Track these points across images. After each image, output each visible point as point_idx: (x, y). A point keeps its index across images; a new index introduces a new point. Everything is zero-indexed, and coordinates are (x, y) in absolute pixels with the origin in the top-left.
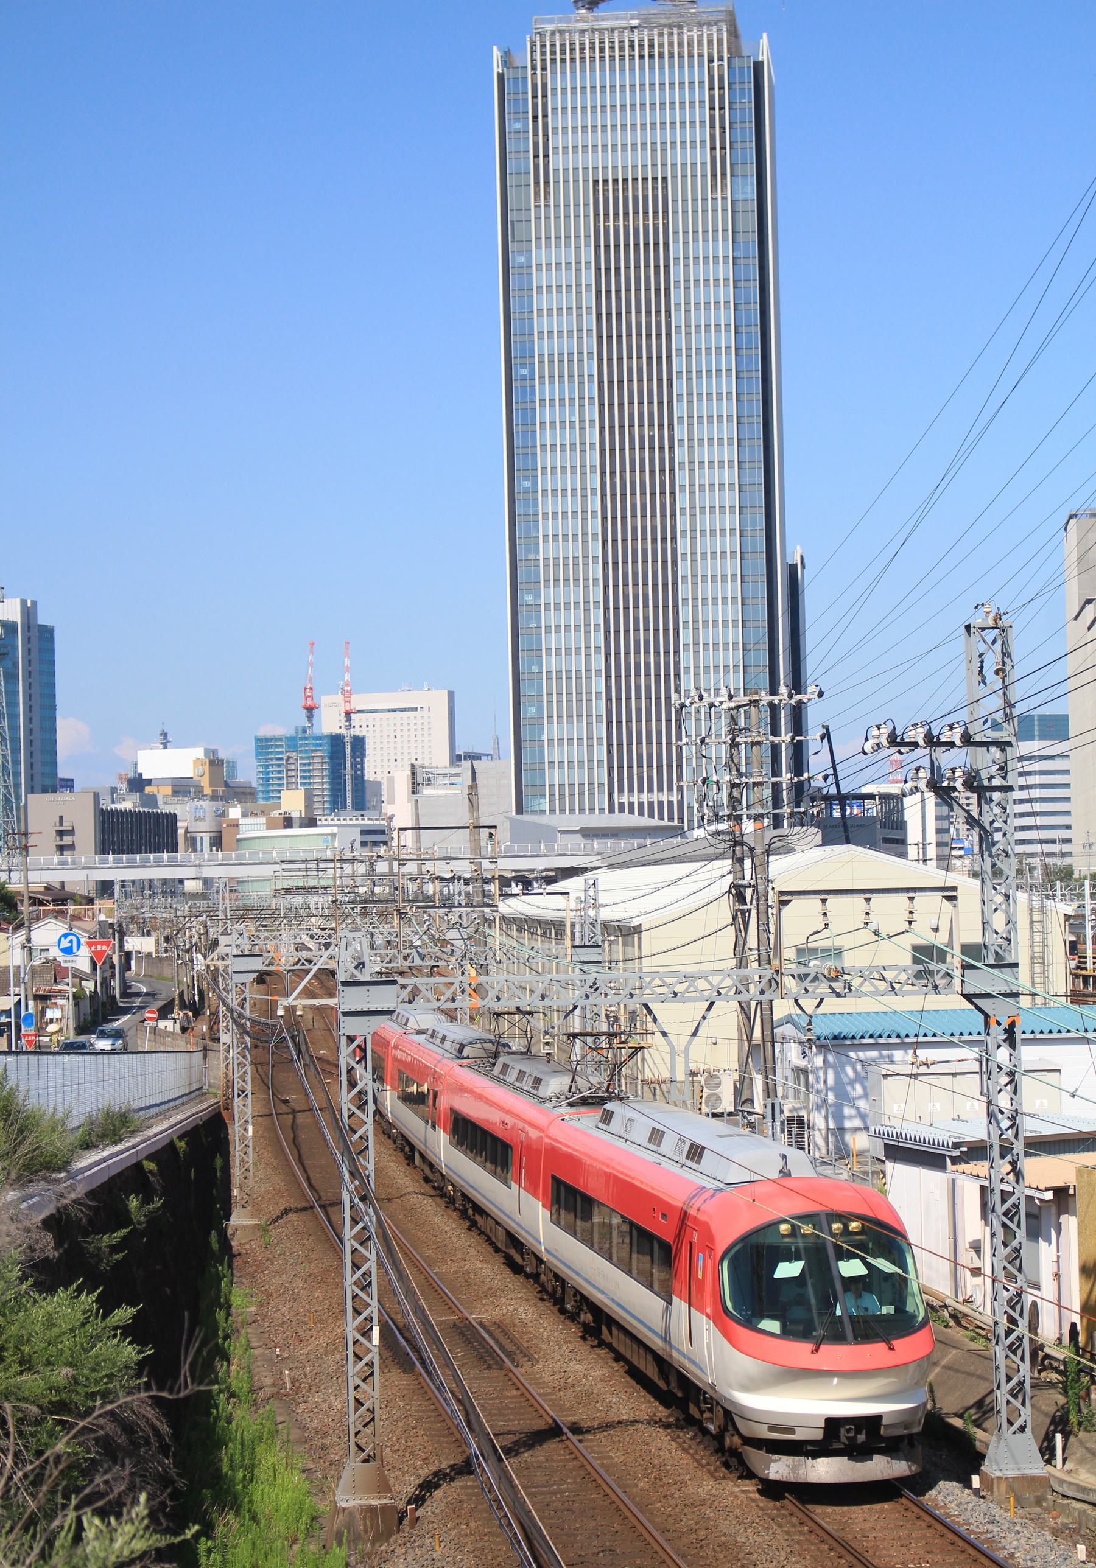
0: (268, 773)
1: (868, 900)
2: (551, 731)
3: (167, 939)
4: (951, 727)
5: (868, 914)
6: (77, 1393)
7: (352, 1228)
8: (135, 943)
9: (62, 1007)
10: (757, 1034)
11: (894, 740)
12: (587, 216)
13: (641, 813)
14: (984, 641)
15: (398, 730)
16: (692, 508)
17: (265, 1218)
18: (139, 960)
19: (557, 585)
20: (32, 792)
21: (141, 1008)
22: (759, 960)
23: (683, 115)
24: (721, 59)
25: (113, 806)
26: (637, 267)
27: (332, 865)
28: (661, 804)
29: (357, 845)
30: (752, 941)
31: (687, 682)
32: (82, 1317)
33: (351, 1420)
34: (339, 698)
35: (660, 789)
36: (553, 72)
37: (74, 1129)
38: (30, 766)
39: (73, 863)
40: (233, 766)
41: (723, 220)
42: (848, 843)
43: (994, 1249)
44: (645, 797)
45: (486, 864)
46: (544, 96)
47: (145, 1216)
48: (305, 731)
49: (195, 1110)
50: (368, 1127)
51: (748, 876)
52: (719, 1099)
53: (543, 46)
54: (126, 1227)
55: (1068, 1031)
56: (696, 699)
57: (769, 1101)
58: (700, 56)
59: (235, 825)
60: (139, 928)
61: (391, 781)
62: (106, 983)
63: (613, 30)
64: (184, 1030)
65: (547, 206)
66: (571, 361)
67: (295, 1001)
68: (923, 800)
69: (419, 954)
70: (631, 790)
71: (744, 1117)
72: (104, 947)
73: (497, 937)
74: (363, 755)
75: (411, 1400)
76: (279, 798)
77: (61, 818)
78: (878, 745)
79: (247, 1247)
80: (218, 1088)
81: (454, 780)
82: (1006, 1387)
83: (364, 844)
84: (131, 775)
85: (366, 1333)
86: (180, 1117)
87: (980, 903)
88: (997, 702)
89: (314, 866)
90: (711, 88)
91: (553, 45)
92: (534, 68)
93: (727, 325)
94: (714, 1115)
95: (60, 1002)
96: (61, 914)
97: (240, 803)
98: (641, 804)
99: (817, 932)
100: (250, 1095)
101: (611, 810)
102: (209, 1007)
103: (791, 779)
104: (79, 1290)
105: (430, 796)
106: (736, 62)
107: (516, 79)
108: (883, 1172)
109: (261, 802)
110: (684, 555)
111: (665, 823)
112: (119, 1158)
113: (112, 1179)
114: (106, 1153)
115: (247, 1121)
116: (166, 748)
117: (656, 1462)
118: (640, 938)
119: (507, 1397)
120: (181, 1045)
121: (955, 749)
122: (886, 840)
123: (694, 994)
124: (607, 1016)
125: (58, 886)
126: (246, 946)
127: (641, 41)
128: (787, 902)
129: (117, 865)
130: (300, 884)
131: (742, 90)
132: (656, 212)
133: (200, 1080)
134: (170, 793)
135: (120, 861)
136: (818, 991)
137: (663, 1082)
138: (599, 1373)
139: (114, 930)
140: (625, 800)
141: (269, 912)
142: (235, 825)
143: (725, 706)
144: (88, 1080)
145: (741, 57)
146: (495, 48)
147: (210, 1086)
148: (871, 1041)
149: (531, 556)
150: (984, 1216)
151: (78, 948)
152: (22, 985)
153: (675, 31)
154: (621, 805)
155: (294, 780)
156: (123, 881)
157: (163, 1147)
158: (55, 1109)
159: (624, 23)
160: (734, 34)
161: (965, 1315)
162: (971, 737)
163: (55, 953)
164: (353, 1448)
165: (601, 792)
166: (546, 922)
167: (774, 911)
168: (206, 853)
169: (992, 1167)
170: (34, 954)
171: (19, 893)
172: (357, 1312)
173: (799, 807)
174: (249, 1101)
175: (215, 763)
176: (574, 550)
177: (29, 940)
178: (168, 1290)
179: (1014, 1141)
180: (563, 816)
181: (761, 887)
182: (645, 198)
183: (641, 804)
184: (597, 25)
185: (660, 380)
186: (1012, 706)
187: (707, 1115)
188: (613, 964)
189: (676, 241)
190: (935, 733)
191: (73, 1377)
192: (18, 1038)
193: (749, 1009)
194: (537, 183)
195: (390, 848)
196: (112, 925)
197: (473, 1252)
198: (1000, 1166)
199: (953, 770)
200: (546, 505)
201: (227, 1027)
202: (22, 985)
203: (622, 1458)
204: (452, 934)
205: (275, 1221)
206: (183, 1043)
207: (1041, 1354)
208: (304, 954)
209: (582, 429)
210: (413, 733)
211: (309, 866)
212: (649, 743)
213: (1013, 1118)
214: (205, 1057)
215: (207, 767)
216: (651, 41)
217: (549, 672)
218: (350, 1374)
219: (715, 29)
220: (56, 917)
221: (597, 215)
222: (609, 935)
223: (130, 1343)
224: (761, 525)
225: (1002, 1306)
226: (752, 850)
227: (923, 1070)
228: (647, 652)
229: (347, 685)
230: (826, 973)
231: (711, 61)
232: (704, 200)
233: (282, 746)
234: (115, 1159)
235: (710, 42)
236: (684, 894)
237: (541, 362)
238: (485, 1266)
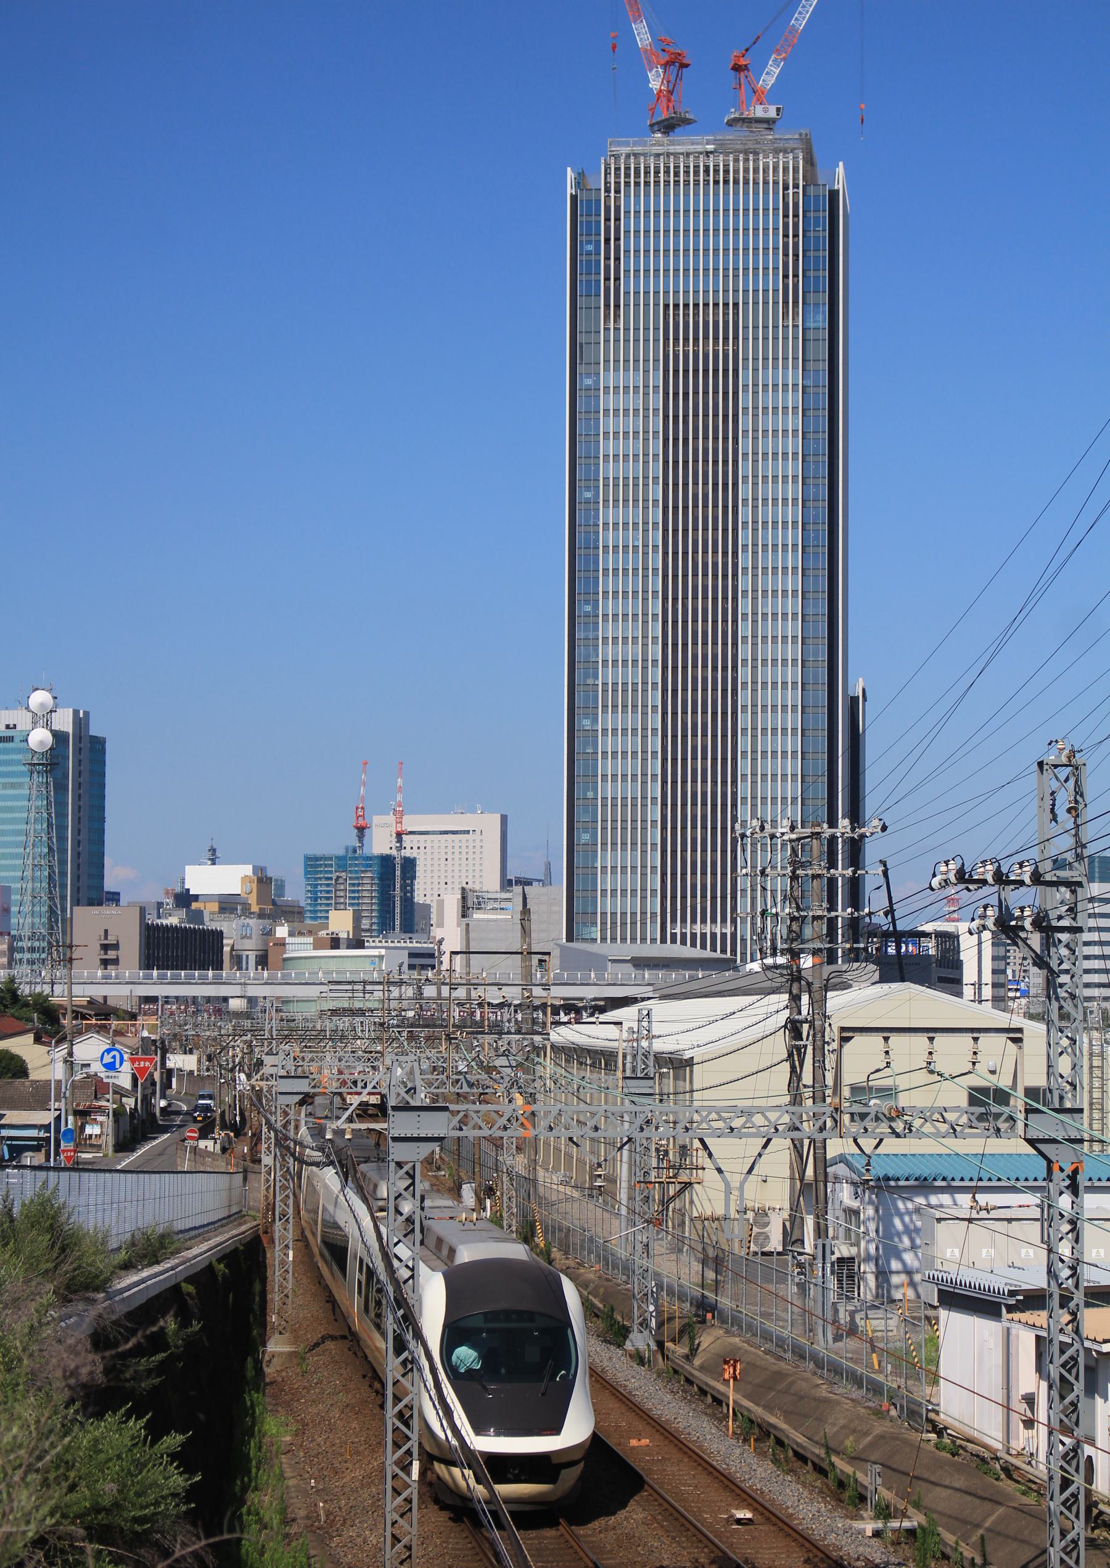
0: (316, 893)
1: (931, 1039)
2: (604, 858)
3: (210, 1058)
5: (930, 1053)
8: (177, 1061)
9: (102, 1124)
10: (810, 1172)
11: (963, 877)
12: (656, 340)
13: (693, 945)
14: (1057, 778)
15: (450, 853)
16: (754, 637)
17: (302, 1346)
20: (78, 905)
21: (180, 1126)
22: (814, 1097)
24: (796, 186)
25: (159, 921)
26: (706, 393)
28: (714, 935)
29: (405, 967)
30: (807, 1078)
33: (388, 1556)
34: (391, 818)
36: (627, 196)
37: (113, 1250)
38: (77, 878)
39: (117, 977)
40: (281, 886)
41: (794, 347)
42: (903, 980)
43: (1050, 1401)
44: (698, 928)
45: (537, 991)
47: (183, 1340)
48: (355, 851)
49: (234, 1232)
51: (804, 1011)
52: (767, 1238)
53: (617, 169)
54: (165, 1351)
55: (999, 1179)
56: (758, 830)
57: (820, 1242)
58: (776, 183)
59: (281, 944)
60: (181, 1045)
61: (441, 904)
62: (146, 1100)
63: (688, 155)
64: (224, 1150)
65: (617, 329)
66: (636, 485)
68: (980, 944)
69: (468, 1082)
72: (147, 1064)
73: (548, 1067)
74: (414, 877)
75: (449, 1537)
76: (327, 918)
77: (106, 931)
78: (945, 881)
79: (284, 1374)
80: (258, 1211)
82: (1059, 1545)
83: (412, 967)
84: (178, 890)
85: (407, 1469)
86: (219, 1239)
88: (1068, 841)
89: (360, 987)
90: (786, 216)
91: (627, 169)
92: (607, 190)
93: (795, 454)
94: (764, 1254)
95: (100, 1118)
96: (102, 1029)
97: (288, 921)
98: (694, 935)
99: (878, 1071)
100: (291, 1220)
101: (663, 940)
102: (251, 1128)
103: (852, 913)
105: (479, 920)
106: (812, 190)
107: (589, 202)
109: (308, 922)
110: (744, 684)
111: (718, 954)
112: (157, 1279)
114: (145, 1274)
115: (287, 1246)
116: (214, 863)
118: (691, 1071)
120: (221, 1165)
121: (1023, 889)
122: (942, 980)
123: (753, 1130)
124: (657, 1150)
126: (290, 1066)
127: (716, 166)
128: (848, 1039)
130: (346, 1005)
132: (726, 339)
133: (240, 1202)
134: (217, 909)
135: (164, 977)
136: (877, 1131)
137: (718, 1219)
138: (641, 1516)
139: (156, 1047)
140: (678, 931)
141: (314, 1033)
143: (786, 837)
144: (129, 1199)
145: (816, 185)
146: (569, 169)
147: (249, 1208)
148: (944, 1184)
149: (590, 681)
150: (1040, 1368)
151: (121, 1064)
152: (63, 1100)
153: (751, 157)
154: (674, 936)
155: (342, 900)
156: (167, 997)
157: (202, 1270)
159: (699, 148)
160: (810, 162)
161: (1017, 1468)
162: (1041, 875)
163: (97, 1068)
166: (596, 1052)
169: (1051, 1317)
170: (75, 1069)
171: (61, 1006)
172: (397, 1446)
174: (290, 1226)
175: (263, 881)
176: (633, 675)
177: (71, 1054)
178: (201, 1416)
180: (643, 945)
181: (817, 1023)
183: (694, 935)
184: (672, 149)
185: (725, 507)
186: (1084, 846)
188: (665, 1097)
189: (746, 368)
190: (1004, 870)
192: (57, 1154)
193: (802, 1147)
194: (607, 306)
195: (439, 972)
196: (154, 1041)
198: (1060, 1316)
199: (1022, 909)
200: (606, 630)
201: (268, 1148)
202: (63, 1100)
204: (501, 1061)
205: (310, 1350)
206: (224, 1164)
207: (1095, 1512)
209: (645, 554)
210: (464, 857)
211: (356, 987)
213: (1073, 1268)
214: (245, 1179)
215: (255, 886)
216: (726, 166)
217: (604, 799)
218: (388, 1509)
219: (791, 156)
220: (98, 1032)
221: (666, 339)
222: (660, 1068)
223: (177, 1468)
224: (823, 656)
225: (1056, 1464)
226: (809, 984)
227: (983, 1214)
229: (400, 806)
230: (887, 1113)
231: (786, 188)
232: (775, 327)
233: (331, 865)
235: (786, 169)
236: (740, 1028)
237: (606, 485)
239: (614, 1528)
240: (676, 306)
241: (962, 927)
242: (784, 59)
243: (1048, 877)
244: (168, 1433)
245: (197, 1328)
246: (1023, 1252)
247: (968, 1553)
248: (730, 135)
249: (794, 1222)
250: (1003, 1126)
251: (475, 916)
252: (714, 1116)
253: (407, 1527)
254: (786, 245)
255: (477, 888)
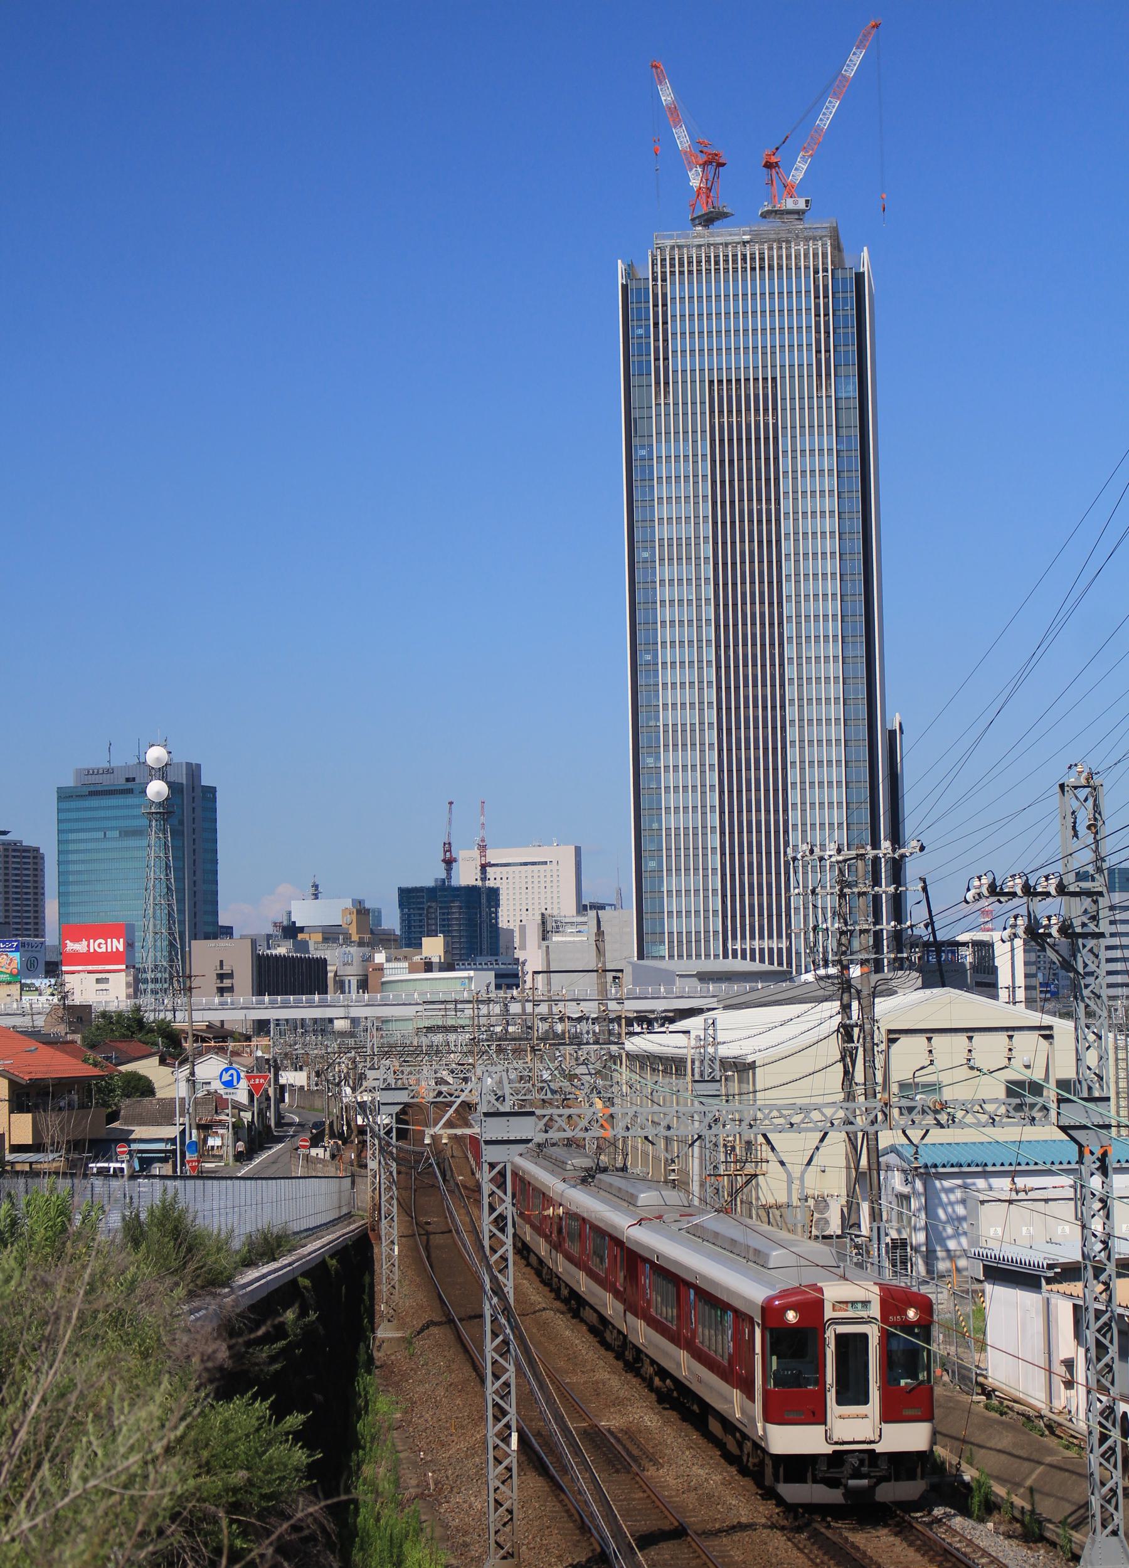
2: (669, 883)
3: (318, 1074)
4: (1047, 878)
5: (1010, 1050)
6: (251, 1493)
7: (493, 1341)
8: (289, 1077)
10: (864, 1162)
11: (994, 890)
12: (703, 413)
13: (753, 959)
14: (1077, 798)
18: (292, 1092)
19: (675, 749)
22: (865, 1094)
23: (754, 322)
24: (825, 270)
25: (269, 952)
26: (749, 459)
27: (471, 1006)
28: (771, 950)
29: (492, 987)
30: (859, 1077)
31: (795, 837)
32: (256, 1424)
33: (491, 1519)
35: (770, 937)
36: (673, 283)
41: (828, 416)
42: (944, 986)
44: (756, 944)
45: (612, 1005)
46: (665, 305)
49: (345, 1231)
50: (508, 1248)
52: (827, 1222)
53: (663, 260)
55: (1036, 1164)
57: (875, 1225)
58: (807, 268)
59: (380, 969)
61: (523, 929)
62: (262, 1114)
63: (726, 245)
64: (333, 1157)
67: (438, 1131)
68: (1012, 950)
70: (743, 937)
71: (852, 1239)
73: (624, 1074)
75: (546, 1501)
77: (221, 962)
79: (393, 1357)
80: (365, 1211)
81: (580, 928)
83: (498, 987)
84: (285, 923)
85: (506, 1440)
87: (1073, 1041)
88: (1088, 856)
89: (453, 1006)
91: (672, 259)
92: (655, 279)
94: (824, 1237)
96: (221, 1051)
98: (753, 951)
101: (725, 956)
104: (254, 1398)
105: (558, 943)
108: (983, 1291)
111: (775, 967)
113: (270, 1295)
115: (392, 1242)
117: (774, 1560)
118: (754, 1074)
119: (634, 1499)
121: (1050, 900)
122: (979, 984)
124: (725, 1146)
125: (219, 1025)
128: (894, 1041)
129: (273, 1005)
130: (440, 1023)
131: (845, 298)
140: (738, 947)
142: (380, 969)
143: (833, 859)
149: (652, 723)
150: (1078, 1335)
154: (735, 951)
158: (220, 1230)
159: (736, 239)
160: (837, 247)
161: (1060, 1425)
163: (216, 1085)
164: (493, 1545)
165: (716, 939)
166: (667, 1058)
167: (883, 1047)
168: (354, 996)
170: (197, 1087)
171: (183, 1031)
172: (497, 1419)
173: (902, 952)
174: (395, 1224)
175: (362, 912)
176: (691, 717)
177: (193, 1074)
179: (1106, 1262)
181: (867, 1027)
182: (756, 396)
184: (712, 240)
186: (1103, 860)
187: (817, 1237)
189: (784, 436)
191: (249, 1480)
192: (183, 1164)
194: (658, 383)
196: (268, 1060)
197: (602, 1363)
199: (1049, 918)
200: (666, 676)
201: (373, 1154)
203: (742, 1557)
204: (582, 1070)
205: (419, 1333)
206: (333, 1169)
208: (444, 1088)
212: (752, 582)
214: (353, 1183)
215: (354, 917)
216: (762, 254)
217: (668, 829)
218: (491, 1477)
219: (820, 243)
220: (217, 1053)
222: (726, 1071)
223: (301, 1448)
226: (859, 992)
227: (1022, 1196)
228: (758, 810)
231: (816, 272)
232: (810, 398)
234: (273, 1276)
235: (815, 255)
237: (661, 546)
238: (613, 1376)
239: (696, 1489)
240: (720, 382)
241: (996, 936)
242: (811, 155)
243: (1072, 888)
244: (290, 1413)
245: (314, 1318)
246: (1060, 1228)
247: (1018, 1501)
248: (765, 226)
249: (852, 1206)
250: (1038, 1115)
251: (554, 939)
252: (775, 1113)
253: (509, 1493)
254: (818, 324)
255: (555, 913)
